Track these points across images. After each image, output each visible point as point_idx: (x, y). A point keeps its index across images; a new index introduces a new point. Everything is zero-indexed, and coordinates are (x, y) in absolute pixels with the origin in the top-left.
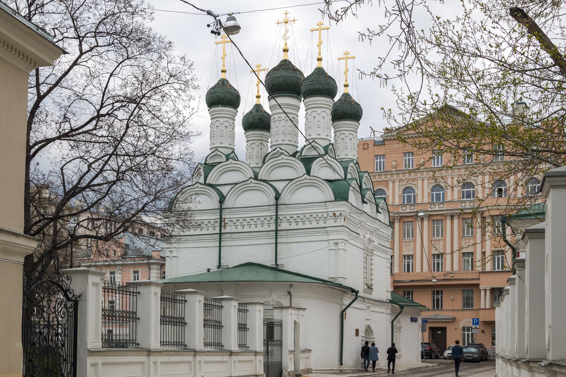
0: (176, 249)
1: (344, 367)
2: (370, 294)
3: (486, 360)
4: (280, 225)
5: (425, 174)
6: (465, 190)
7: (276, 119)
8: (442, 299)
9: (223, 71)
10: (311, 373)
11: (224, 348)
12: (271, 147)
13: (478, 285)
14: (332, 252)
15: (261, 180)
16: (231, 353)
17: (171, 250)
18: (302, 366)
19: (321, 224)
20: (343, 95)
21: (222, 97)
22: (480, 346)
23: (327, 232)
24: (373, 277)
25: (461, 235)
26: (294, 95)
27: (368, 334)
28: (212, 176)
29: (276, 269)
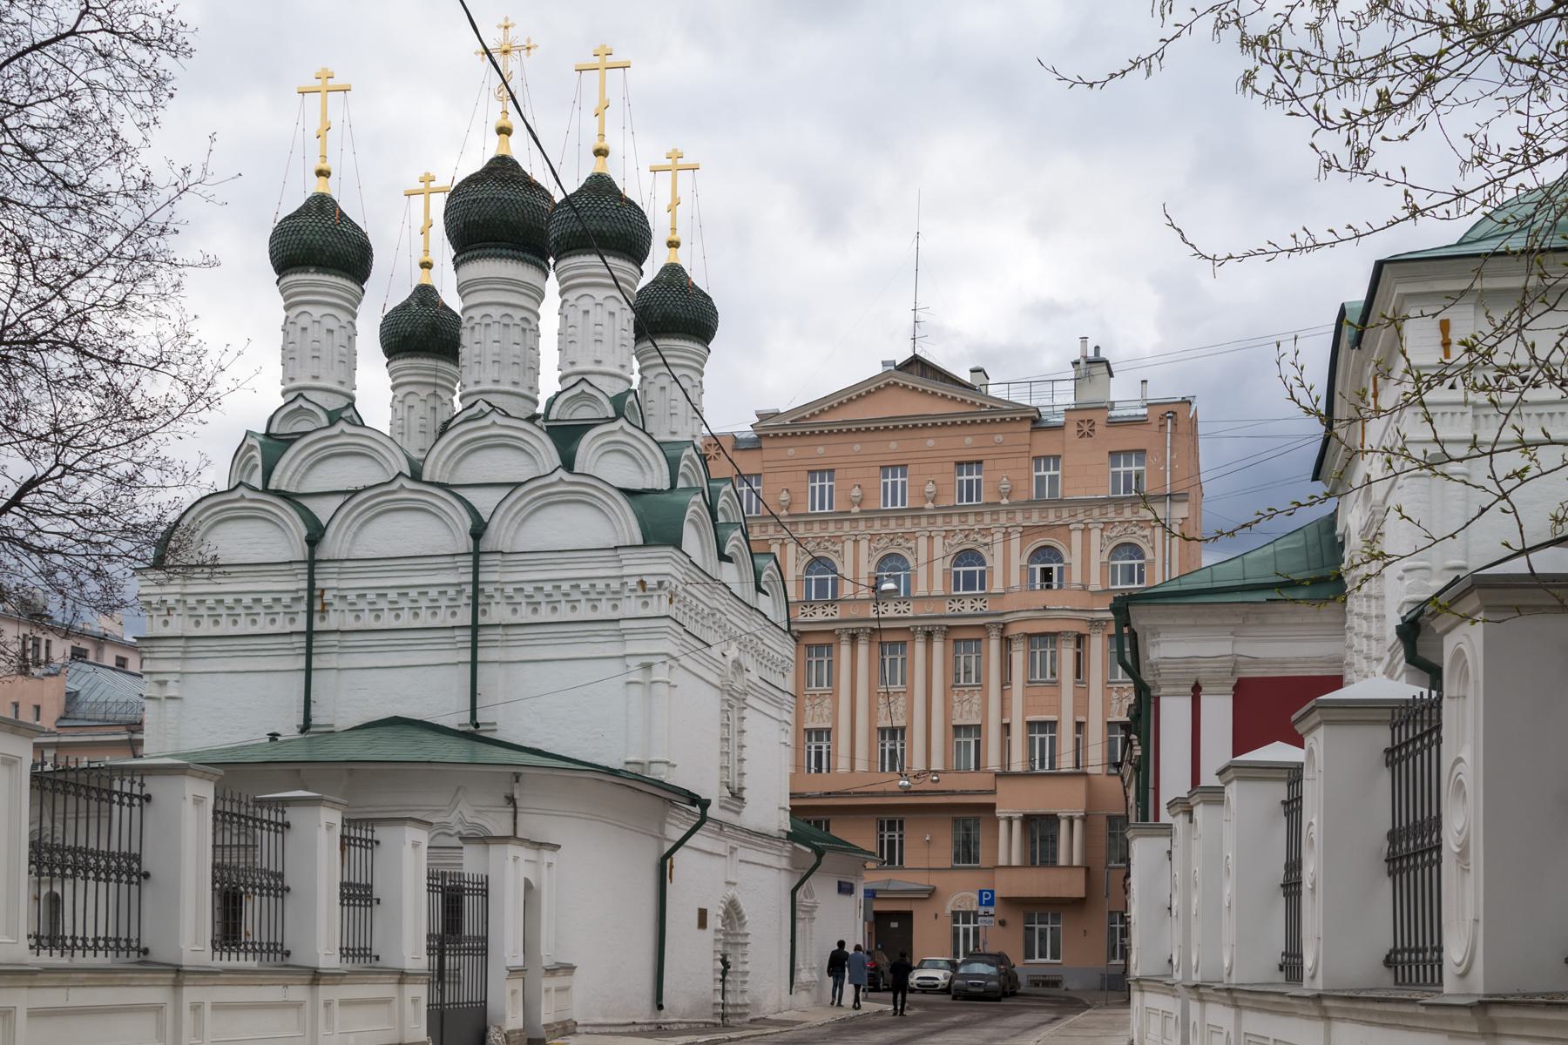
0: (177, 677)
1: (665, 1017)
2: (738, 813)
3: (1014, 994)
4: (484, 612)
5: (862, 525)
6: (961, 569)
7: (477, 319)
8: (901, 843)
9: (322, 173)
10: (574, 1033)
11: (291, 961)
12: (461, 399)
13: (992, 807)
14: (636, 689)
15: (431, 483)
16: (316, 977)
17: (161, 678)
18: (547, 1015)
19: (605, 611)
20: (665, 269)
21: (318, 247)
22: (999, 959)
23: (621, 634)
24: (746, 767)
25: (951, 681)
26: (528, 256)
27: (731, 924)
28: (285, 469)
29: (473, 735)
